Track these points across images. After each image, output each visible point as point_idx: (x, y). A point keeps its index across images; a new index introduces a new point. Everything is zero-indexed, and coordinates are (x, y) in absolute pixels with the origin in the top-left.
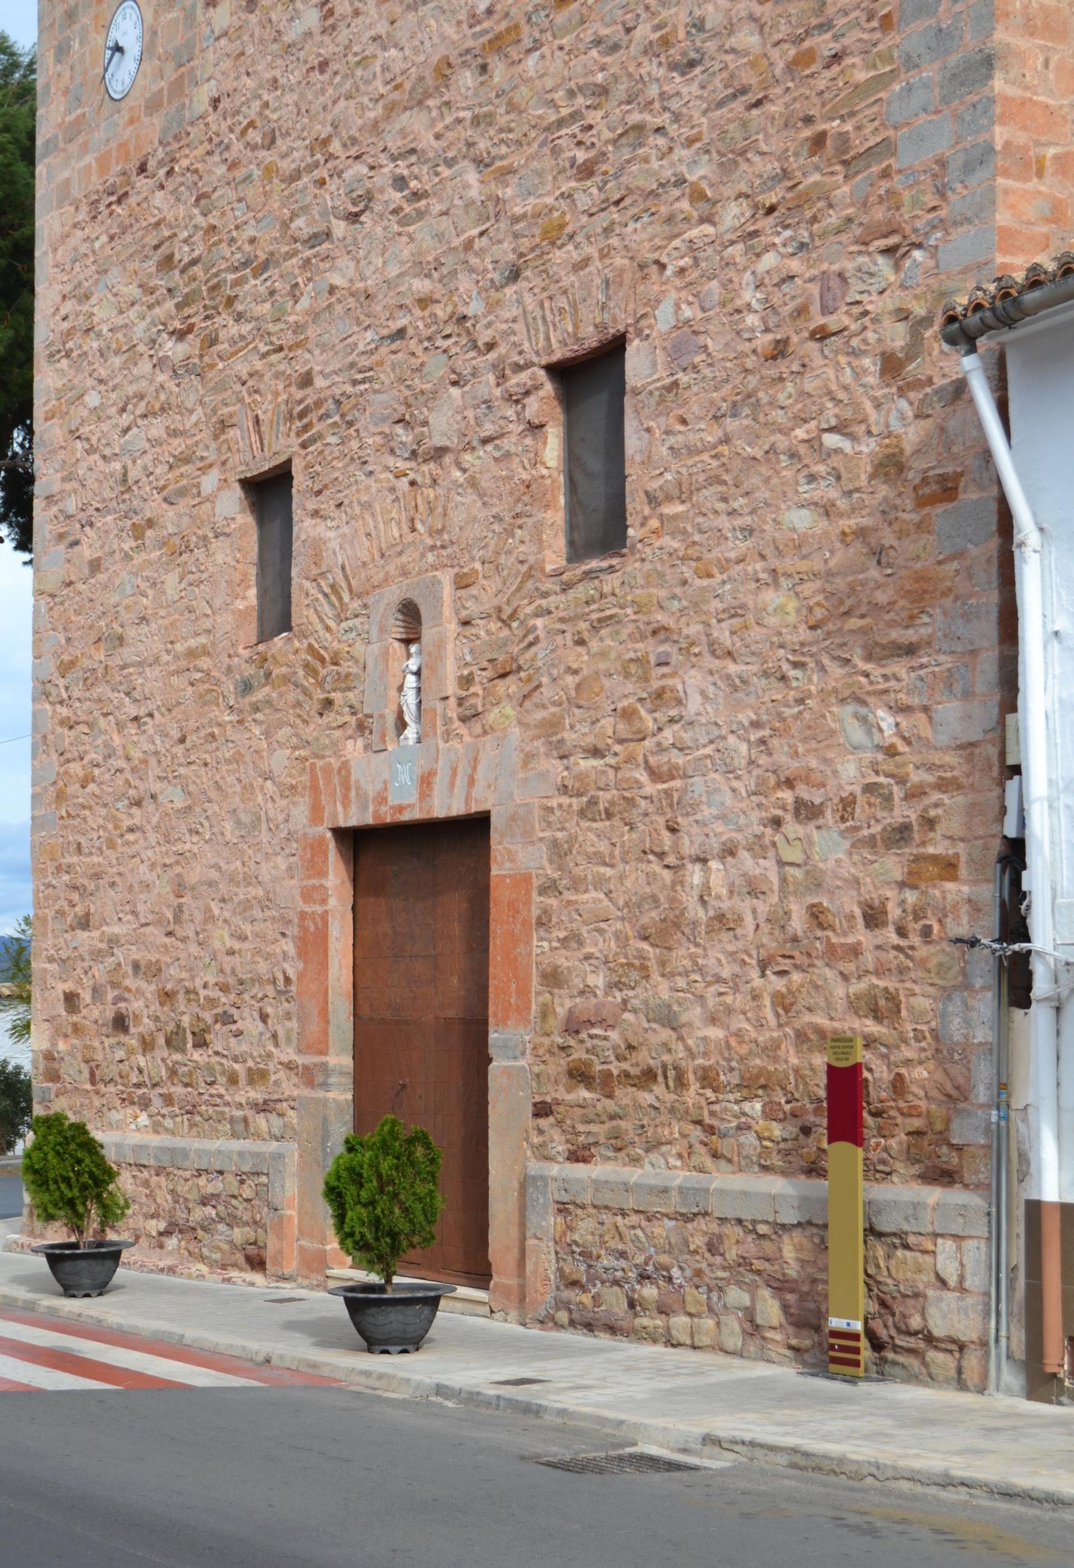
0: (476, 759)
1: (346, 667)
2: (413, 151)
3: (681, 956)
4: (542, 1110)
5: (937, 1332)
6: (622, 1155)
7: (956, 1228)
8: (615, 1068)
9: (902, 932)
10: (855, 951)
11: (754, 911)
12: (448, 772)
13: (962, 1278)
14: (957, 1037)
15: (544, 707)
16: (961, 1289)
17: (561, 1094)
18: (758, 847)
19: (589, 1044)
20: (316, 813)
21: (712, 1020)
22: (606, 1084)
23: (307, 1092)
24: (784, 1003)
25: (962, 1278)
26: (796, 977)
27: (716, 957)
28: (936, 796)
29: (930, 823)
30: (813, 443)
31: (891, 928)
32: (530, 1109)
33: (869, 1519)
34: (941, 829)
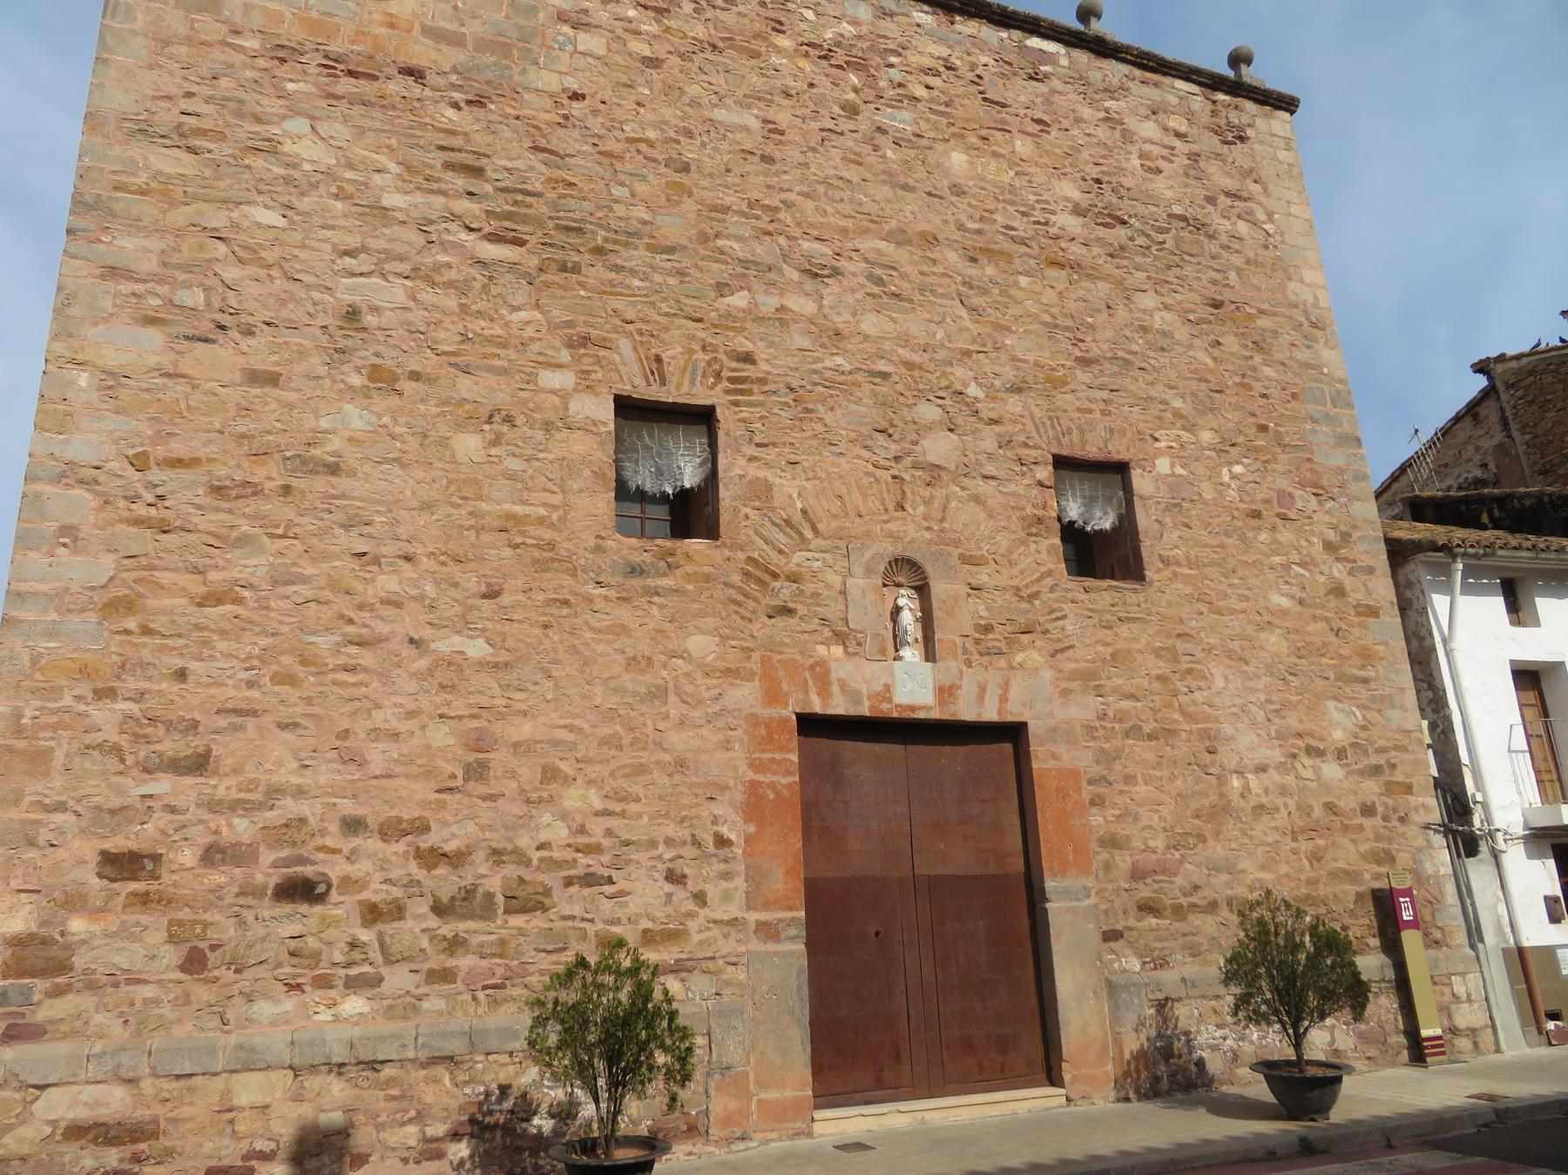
0: (1007, 684)
1: (809, 587)
2: (528, 802)
3: (1231, 829)
4: (1111, 936)
5: (1462, 1026)
6: (1197, 959)
7: (1461, 969)
8: (1184, 901)
9: (1385, 819)
10: (1361, 828)
11: (1285, 805)
12: (974, 690)
13: (1469, 996)
14: (1430, 872)
15: (1076, 661)
16: (1469, 1000)
17: (1132, 922)
18: (1281, 767)
19: (1156, 886)
20: (773, 695)
21: (1263, 868)
22: (1179, 912)
23: (771, 947)
24: (1316, 857)
25: (1469, 996)
26: (1320, 842)
27: (1262, 829)
28: (1394, 753)
29: (1393, 766)
30: (1286, 567)
31: (1379, 818)
32: (1099, 938)
33: (320, 869)
34: (1400, 768)
